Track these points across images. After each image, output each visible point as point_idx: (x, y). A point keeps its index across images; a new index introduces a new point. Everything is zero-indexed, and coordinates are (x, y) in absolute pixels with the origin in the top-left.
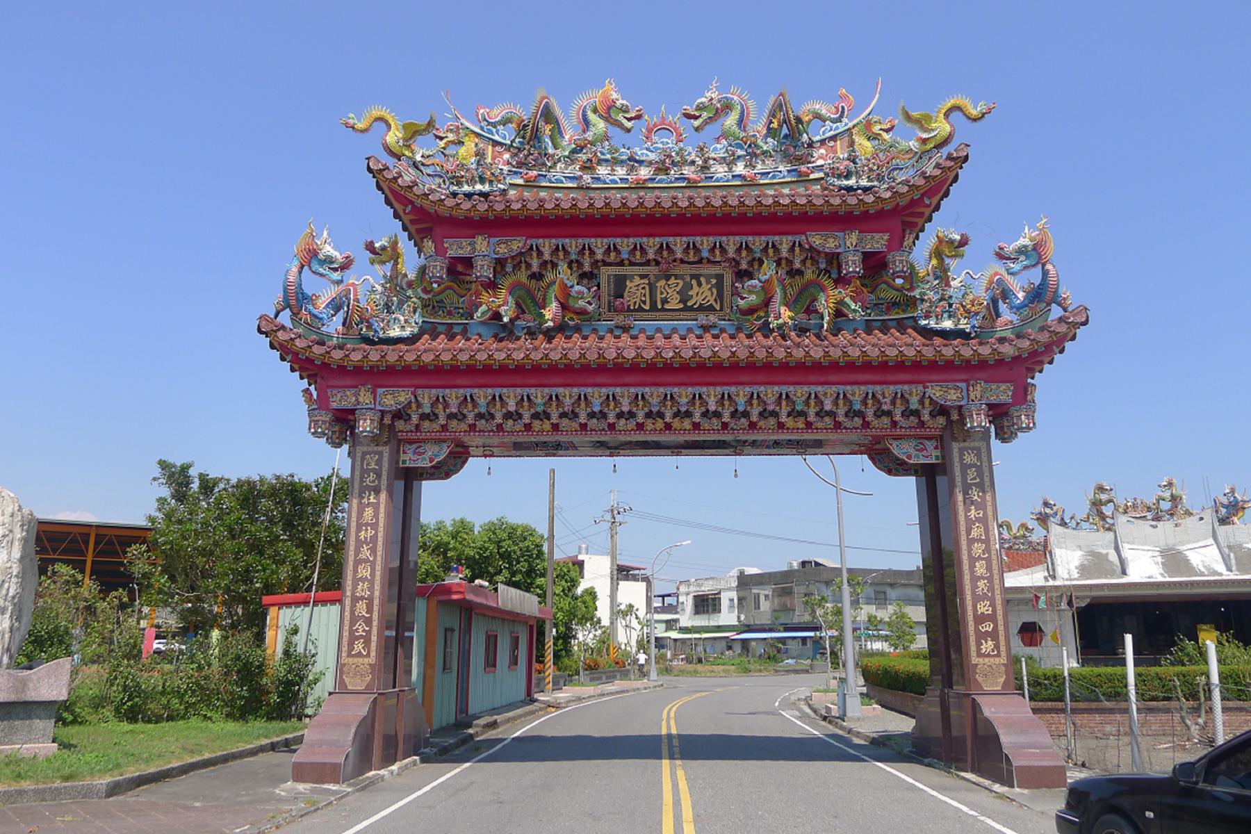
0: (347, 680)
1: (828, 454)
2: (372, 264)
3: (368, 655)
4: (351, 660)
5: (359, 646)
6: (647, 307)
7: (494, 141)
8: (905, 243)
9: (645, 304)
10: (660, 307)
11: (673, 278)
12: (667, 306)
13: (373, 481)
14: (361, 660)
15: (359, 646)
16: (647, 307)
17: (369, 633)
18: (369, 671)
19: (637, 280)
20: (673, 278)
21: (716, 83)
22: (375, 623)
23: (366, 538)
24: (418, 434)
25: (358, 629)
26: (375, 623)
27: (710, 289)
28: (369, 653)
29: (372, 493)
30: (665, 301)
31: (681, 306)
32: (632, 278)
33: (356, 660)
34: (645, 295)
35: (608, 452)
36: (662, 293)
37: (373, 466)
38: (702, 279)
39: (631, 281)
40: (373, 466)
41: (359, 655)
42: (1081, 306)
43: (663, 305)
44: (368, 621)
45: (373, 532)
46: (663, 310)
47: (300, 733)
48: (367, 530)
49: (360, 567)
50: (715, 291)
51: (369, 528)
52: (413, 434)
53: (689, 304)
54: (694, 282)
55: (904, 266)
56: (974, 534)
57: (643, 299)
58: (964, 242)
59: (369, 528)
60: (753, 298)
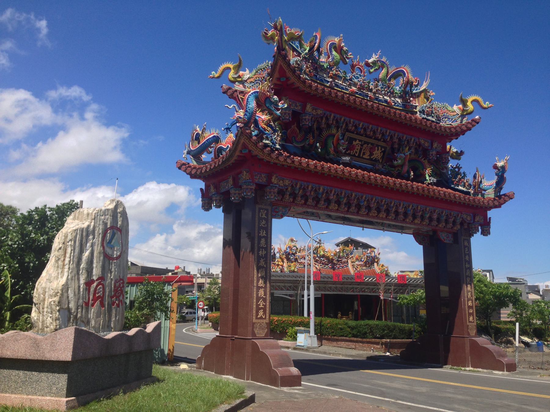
0: (256, 332)
1: (297, 218)
2: (461, 151)
3: (265, 318)
4: (257, 321)
5: (261, 313)
6: (357, 155)
7: (293, 47)
8: (434, 146)
9: (356, 153)
10: (361, 156)
11: (370, 144)
12: (364, 157)
13: (264, 225)
14: (262, 321)
15: (261, 313)
16: (357, 155)
17: (265, 306)
18: (266, 327)
19: (357, 142)
20: (370, 144)
21: (380, 53)
22: (268, 301)
23: (262, 255)
24: (281, 202)
25: (260, 304)
26: (268, 301)
27: (381, 153)
28: (266, 317)
29: (264, 231)
30: (364, 154)
31: (369, 157)
32: (355, 140)
33: (259, 321)
34: (358, 150)
35: (382, 228)
36: (364, 150)
37: (264, 216)
38: (380, 148)
39: (355, 142)
40: (264, 216)
41: (261, 318)
42: (512, 192)
43: (363, 155)
44: (265, 300)
45: (265, 252)
46: (362, 158)
47: (292, 362)
48: (262, 251)
49: (260, 270)
50: (382, 153)
51: (263, 250)
52: (279, 202)
53: (372, 157)
54: (376, 148)
55: (433, 157)
56: (467, 274)
57: (357, 151)
58: (462, 153)
59: (263, 250)
60: (400, 161)
